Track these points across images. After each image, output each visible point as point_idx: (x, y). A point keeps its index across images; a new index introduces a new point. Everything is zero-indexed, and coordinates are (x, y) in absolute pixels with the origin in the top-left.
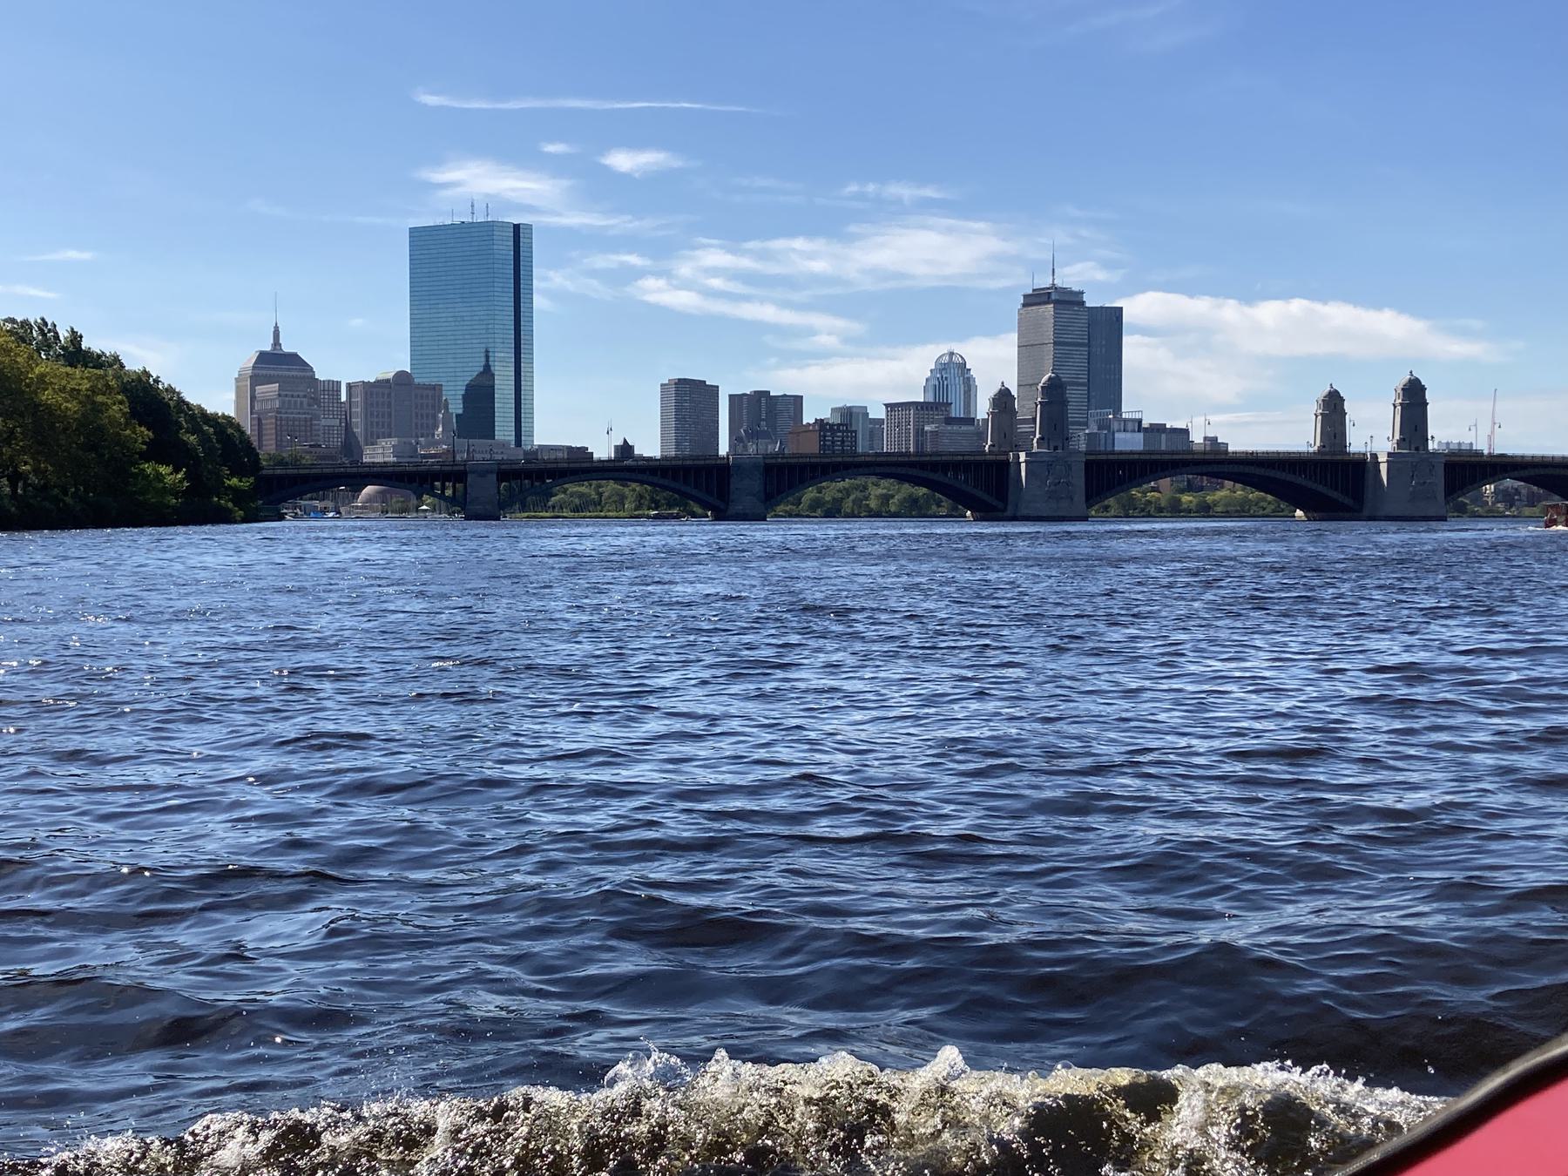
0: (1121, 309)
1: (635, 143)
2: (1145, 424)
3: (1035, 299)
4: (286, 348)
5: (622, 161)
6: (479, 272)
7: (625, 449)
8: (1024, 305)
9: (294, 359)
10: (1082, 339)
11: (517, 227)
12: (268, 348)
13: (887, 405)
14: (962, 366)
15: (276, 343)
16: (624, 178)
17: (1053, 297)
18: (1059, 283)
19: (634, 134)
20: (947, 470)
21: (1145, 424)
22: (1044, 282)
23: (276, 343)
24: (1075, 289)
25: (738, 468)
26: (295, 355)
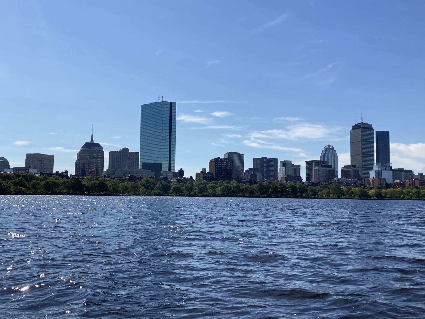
0: (389, 132)
1: (220, 110)
2: (393, 168)
3: (356, 127)
4: (95, 142)
5: (217, 114)
6: (160, 119)
7: (91, 152)
8: (352, 129)
9: (97, 145)
10: (371, 142)
11: (171, 104)
12: (90, 142)
13: (306, 162)
14: (333, 149)
15: (92, 140)
16: (219, 118)
17: (362, 126)
18: (364, 122)
19: (220, 108)
20: (320, 182)
21: (393, 168)
22: (359, 122)
23: (92, 140)
24: (369, 123)
25: (226, 177)
26: (98, 144)
